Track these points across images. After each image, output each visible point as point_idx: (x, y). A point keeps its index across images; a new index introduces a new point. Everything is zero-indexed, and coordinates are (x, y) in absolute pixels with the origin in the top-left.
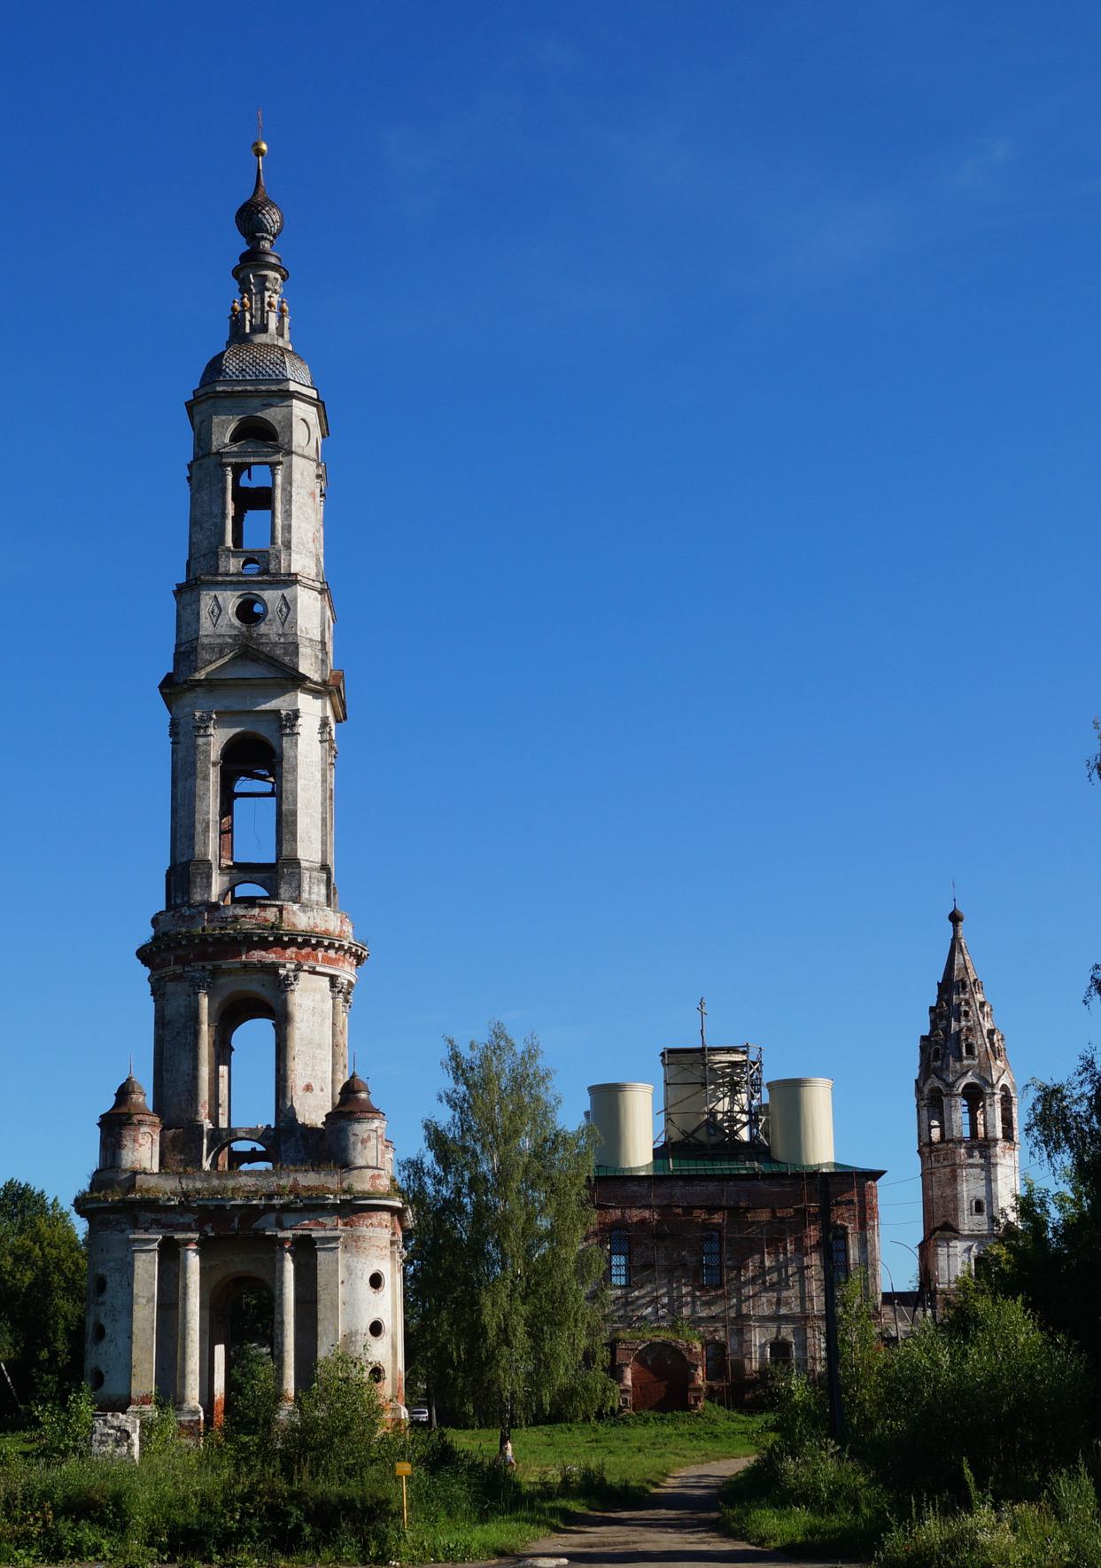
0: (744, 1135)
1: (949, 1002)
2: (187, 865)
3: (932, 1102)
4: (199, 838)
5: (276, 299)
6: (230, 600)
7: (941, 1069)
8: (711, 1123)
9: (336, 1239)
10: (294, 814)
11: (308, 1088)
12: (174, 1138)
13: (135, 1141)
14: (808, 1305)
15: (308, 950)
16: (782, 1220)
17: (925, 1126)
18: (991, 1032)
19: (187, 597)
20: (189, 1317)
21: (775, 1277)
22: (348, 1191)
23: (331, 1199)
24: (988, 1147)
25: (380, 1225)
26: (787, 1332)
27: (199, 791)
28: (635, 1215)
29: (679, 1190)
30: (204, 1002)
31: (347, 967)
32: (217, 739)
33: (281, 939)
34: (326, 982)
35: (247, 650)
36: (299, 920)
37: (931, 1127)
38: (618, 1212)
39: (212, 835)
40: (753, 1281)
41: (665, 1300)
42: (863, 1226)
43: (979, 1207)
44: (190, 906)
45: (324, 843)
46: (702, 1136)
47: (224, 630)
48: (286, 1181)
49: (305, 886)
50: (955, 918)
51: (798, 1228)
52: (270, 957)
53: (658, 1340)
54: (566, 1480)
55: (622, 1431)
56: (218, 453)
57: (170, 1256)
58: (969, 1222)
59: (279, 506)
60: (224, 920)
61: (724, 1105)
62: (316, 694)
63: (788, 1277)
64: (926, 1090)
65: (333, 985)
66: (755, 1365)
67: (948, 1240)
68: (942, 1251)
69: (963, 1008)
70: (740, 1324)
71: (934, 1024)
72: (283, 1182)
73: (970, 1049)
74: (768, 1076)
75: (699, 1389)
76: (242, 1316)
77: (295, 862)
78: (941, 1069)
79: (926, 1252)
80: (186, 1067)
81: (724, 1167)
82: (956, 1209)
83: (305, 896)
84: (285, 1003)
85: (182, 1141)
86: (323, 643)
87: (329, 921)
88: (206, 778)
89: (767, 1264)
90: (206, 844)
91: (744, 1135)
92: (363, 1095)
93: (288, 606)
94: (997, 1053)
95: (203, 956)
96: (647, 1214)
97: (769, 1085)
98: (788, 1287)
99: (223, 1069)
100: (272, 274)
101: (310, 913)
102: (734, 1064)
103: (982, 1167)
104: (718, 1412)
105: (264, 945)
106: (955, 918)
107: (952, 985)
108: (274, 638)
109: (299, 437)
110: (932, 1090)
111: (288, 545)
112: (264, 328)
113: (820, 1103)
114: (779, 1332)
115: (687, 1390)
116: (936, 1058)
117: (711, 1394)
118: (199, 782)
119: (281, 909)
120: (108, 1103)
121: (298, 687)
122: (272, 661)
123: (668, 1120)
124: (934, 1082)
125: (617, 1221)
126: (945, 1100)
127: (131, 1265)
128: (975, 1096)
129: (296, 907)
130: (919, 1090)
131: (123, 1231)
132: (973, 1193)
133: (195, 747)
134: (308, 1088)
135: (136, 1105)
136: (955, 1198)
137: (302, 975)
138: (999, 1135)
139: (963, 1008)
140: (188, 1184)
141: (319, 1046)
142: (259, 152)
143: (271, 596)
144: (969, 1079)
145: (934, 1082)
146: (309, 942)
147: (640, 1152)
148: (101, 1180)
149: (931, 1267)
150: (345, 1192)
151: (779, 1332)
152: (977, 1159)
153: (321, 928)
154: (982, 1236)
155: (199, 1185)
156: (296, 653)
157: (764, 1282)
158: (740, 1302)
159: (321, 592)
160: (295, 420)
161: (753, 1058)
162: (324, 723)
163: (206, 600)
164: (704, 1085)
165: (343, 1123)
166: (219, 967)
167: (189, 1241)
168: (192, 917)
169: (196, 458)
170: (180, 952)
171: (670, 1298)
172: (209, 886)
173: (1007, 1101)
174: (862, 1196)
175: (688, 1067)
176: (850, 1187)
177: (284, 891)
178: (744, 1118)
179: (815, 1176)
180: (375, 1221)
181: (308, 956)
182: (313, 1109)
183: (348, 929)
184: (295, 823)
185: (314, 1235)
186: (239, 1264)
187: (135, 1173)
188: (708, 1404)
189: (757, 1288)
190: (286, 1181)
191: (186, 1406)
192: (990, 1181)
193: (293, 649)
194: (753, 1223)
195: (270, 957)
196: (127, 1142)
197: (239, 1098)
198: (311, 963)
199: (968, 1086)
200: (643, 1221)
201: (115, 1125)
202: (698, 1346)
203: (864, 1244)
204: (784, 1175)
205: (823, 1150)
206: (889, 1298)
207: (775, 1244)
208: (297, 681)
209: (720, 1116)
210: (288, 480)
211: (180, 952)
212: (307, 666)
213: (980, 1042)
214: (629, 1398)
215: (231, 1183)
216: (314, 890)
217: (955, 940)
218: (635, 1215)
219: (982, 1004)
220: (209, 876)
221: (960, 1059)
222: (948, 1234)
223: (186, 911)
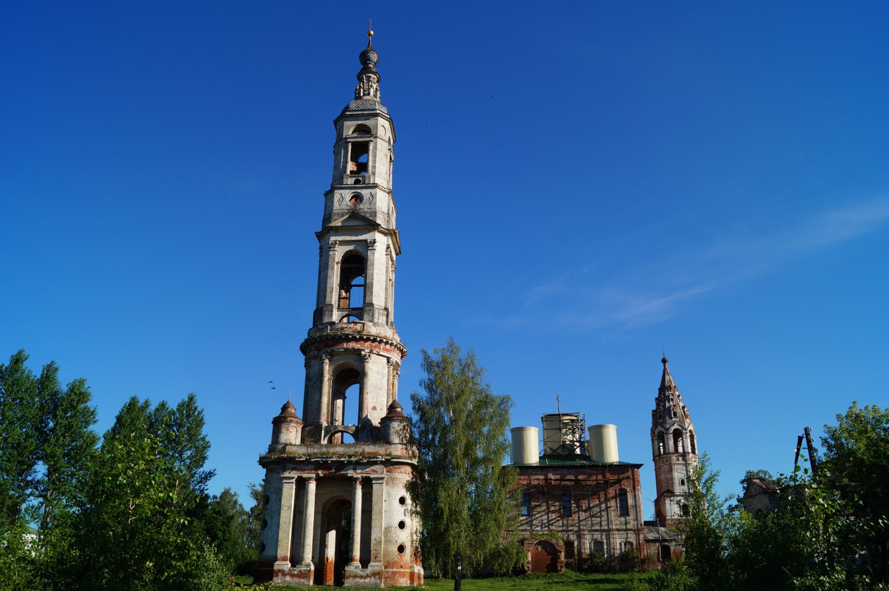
0: (578, 451)
1: (664, 395)
2: (322, 308)
3: (659, 436)
4: (328, 295)
5: (375, 86)
6: (348, 194)
8: (564, 445)
9: (383, 478)
10: (372, 284)
11: (374, 408)
12: (309, 431)
13: (288, 430)
15: (377, 343)
18: (683, 408)
19: (329, 196)
20: (308, 517)
22: (390, 455)
23: (380, 458)
25: (405, 473)
27: (329, 275)
30: (327, 368)
31: (395, 354)
32: (338, 253)
33: (362, 338)
34: (385, 360)
35: (354, 215)
36: (372, 330)
39: (334, 293)
44: (322, 324)
45: (386, 299)
46: (560, 451)
47: (344, 207)
48: (359, 449)
49: (376, 316)
50: (664, 361)
52: (357, 346)
54: (779, 480)
55: (528, 581)
56: (346, 138)
57: (301, 485)
58: (678, 489)
59: (371, 153)
60: (337, 329)
61: (570, 437)
62: (385, 234)
65: (388, 362)
66: (588, 551)
71: (658, 405)
72: (357, 450)
73: (675, 414)
74: (587, 425)
75: (562, 562)
76: (335, 515)
77: (372, 305)
79: (659, 504)
80: (317, 398)
81: (568, 463)
82: (672, 483)
83: (376, 320)
84: (364, 367)
85: (312, 430)
86: (388, 214)
87: (388, 332)
88: (333, 269)
90: (331, 297)
92: (399, 410)
93: (373, 196)
94: (686, 416)
95: (327, 346)
97: (589, 429)
99: (339, 402)
100: (373, 76)
101: (379, 327)
102: (573, 421)
104: (573, 575)
105: (354, 339)
106: (664, 361)
107: (664, 388)
108: (366, 210)
109: (381, 132)
111: (374, 174)
112: (369, 94)
113: (611, 434)
116: (660, 418)
117: (567, 565)
118: (329, 270)
119: (364, 324)
120: (278, 413)
121: (375, 230)
122: (364, 219)
123: (544, 444)
124: (660, 428)
127: (281, 490)
128: (678, 434)
129: (371, 324)
130: (653, 432)
131: (278, 473)
133: (329, 256)
134: (374, 408)
135: (290, 413)
136: (672, 479)
137: (373, 356)
140: (311, 451)
141: (380, 389)
142: (370, 35)
143: (365, 193)
144: (676, 426)
145: (660, 428)
146: (376, 340)
147: (533, 456)
148: (272, 449)
149: (662, 509)
150: (387, 455)
153: (383, 334)
155: (316, 451)
156: (376, 216)
159: (389, 193)
160: (379, 126)
161: (581, 418)
162: (388, 247)
163: (337, 194)
164: (560, 429)
165: (388, 422)
166: (333, 351)
167: (310, 479)
168: (323, 329)
169: (337, 142)
170: (317, 345)
172: (332, 315)
173: (692, 437)
174: (633, 475)
175: (552, 422)
176: (626, 470)
177: (366, 317)
178: (578, 444)
179: (612, 467)
180: (402, 470)
181: (376, 347)
182: (376, 417)
183: (398, 339)
184: (372, 288)
185: (371, 476)
186: (337, 492)
187: (286, 445)
190: (359, 449)
191: (304, 563)
193: (375, 214)
195: (357, 346)
196: (284, 430)
197: (339, 412)
198: (377, 350)
199: (675, 430)
201: (279, 423)
202: (561, 543)
204: (598, 466)
205: (613, 456)
206: (646, 523)
208: (374, 226)
210: (375, 148)
211: (317, 345)
212: (380, 220)
213: (679, 411)
214: (530, 566)
215: (331, 450)
216: (381, 318)
220: (332, 311)
221: (671, 418)
223: (320, 327)
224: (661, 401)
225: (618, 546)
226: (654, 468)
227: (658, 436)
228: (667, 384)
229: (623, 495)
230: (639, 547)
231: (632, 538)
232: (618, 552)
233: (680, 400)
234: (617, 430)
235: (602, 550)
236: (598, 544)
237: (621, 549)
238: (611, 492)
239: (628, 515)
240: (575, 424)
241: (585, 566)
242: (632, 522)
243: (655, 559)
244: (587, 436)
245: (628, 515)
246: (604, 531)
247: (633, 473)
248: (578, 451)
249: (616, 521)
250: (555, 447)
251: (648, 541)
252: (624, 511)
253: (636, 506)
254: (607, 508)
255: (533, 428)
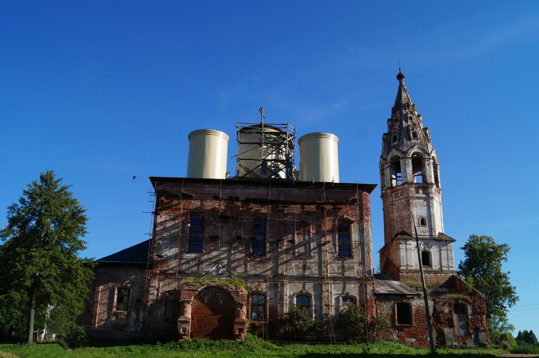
7: (398, 145)
14: (324, 269)
16: (308, 213)
17: (388, 178)
18: (425, 129)
21: (302, 250)
24: (428, 188)
26: (309, 287)
28: (209, 204)
29: (239, 191)
37: (392, 179)
38: (198, 203)
40: (287, 251)
41: (225, 262)
42: (361, 220)
43: (423, 222)
50: (400, 77)
51: (319, 217)
53: (213, 284)
63: (310, 251)
64: (389, 158)
66: (286, 310)
67: (406, 240)
68: (402, 246)
69: (410, 115)
70: (277, 281)
71: (391, 127)
73: (415, 135)
75: (243, 323)
78: (398, 145)
82: (409, 223)
89: (297, 240)
91: (282, 175)
96: (215, 204)
98: (310, 257)
103: (424, 199)
104: (256, 342)
106: (400, 77)
107: (399, 107)
110: (392, 158)
113: (331, 146)
114: (304, 287)
115: (233, 323)
116: (395, 139)
117: (253, 329)
124: (395, 152)
125: (197, 209)
126: (402, 162)
132: (419, 214)
136: (410, 216)
138: (433, 182)
139: (410, 115)
144: (415, 150)
145: (395, 152)
149: (393, 257)
151: (304, 287)
152: (421, 194)
154: (426, 239)
157: (294, 253)
158: (277, 265)
164: (260, 144)
171: (229, 260)
175: (248, 135)
176: (349, 193)
179: (330, 186)
188: (250, 336)
189: (289, 257)
192: (429, 207)
194: (288, 214)
200: (214, 210)
203: (362, 231)
205: (332, 173)
207: (303, 226)
209: (269, 164)
217: (401, 86)
218: (209, 204)
219: (419, 116)
221: (410, 139)
222: (406, 237)
224: (396, 120)
225: (333, 302)
226: (382, 207)
227: (392, 163)
228: (404, 101)
229: (343, 229)
230: (364, 305)
231: (353, 289)
232: (332, 312)
233: (421, 119)
234: (339, 144)
235: (309, 306)
236: (303, 297)
237: (337, 307)
238: (328, 224)
239: (351, 256)
240: (278, 140)
241: (277, 329)
242: (357, 267)
243: (388, 322)
244: (296, 155)
245: (351, 256)
246: (309, 279)
247: (360, 196)
248: (282, 175)
249: (333, 269)
250: (251, 166)
251: (380, 297)
252: (345, 252)
253: (362, 244)
254: (320, 246)
255: (222, 134)
